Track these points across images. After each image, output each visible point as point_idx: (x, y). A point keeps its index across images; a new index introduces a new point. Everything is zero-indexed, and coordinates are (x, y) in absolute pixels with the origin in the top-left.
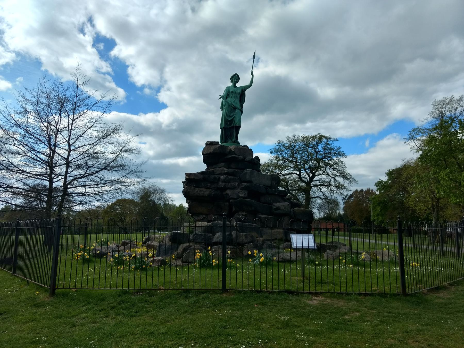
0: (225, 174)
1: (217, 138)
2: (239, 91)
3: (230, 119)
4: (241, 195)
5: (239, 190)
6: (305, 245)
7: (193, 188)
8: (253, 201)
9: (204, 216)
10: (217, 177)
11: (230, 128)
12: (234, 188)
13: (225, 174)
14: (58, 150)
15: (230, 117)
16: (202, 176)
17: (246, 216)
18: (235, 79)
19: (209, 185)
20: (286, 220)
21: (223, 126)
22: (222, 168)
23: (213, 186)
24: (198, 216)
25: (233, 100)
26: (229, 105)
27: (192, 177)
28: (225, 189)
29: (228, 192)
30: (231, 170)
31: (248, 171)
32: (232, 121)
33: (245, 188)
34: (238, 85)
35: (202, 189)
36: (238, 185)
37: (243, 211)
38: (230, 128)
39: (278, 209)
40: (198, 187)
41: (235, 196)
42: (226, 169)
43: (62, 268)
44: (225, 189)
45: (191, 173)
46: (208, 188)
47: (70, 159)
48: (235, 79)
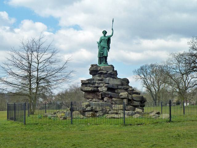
0: (99, 80)
1: (96, 61)
2: (107, 38)
3: (102, 53)
4: (104, 90)
5: (104, 87)
6: (138, 109)
7: (84, 87)
8: (110, 92)
9: (91, 99)
10: (95, 81)
11: (103, 58)
12: (101, 87)
13: (99, 80)
14: (33, 64)
15: (102, 52)
16: (88, 81)
17: (107, 99)
18: (105, 33)
19: (91, 85)
20: (125, 101)
21: (99, 56)
22: (97, 77)
23: (93, 86)
24: (89, 99)
25: (104, 44)
26: (101, 46)
27: (83, 82)
28: (98, 87)
29: (99, 88)
30: (100, 78)
31: (108, 78)
32: (103, 54)
33: (106, 87)
34: (106, 35)
35: (88, 87)
36: (104, 85)
37: (106, 97)
38: (103, 58)
39: (121, 96)
40: (86, 86)
41: (102, 91)
42: (98, 78)
43: (168, 111)
44: (98, 87)
45: (83, 80)
46: (91, 87)
47: (38, 68)
48: (105, 33)
